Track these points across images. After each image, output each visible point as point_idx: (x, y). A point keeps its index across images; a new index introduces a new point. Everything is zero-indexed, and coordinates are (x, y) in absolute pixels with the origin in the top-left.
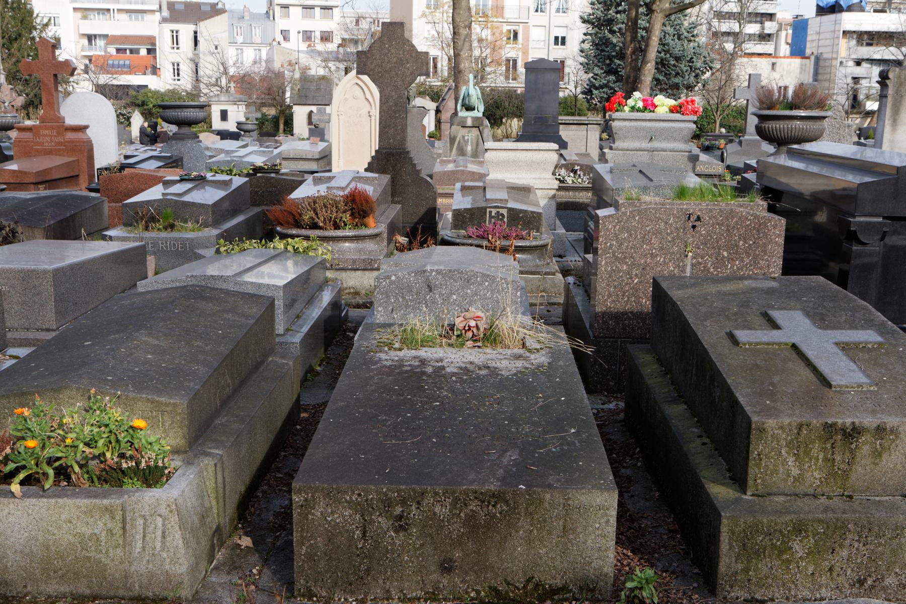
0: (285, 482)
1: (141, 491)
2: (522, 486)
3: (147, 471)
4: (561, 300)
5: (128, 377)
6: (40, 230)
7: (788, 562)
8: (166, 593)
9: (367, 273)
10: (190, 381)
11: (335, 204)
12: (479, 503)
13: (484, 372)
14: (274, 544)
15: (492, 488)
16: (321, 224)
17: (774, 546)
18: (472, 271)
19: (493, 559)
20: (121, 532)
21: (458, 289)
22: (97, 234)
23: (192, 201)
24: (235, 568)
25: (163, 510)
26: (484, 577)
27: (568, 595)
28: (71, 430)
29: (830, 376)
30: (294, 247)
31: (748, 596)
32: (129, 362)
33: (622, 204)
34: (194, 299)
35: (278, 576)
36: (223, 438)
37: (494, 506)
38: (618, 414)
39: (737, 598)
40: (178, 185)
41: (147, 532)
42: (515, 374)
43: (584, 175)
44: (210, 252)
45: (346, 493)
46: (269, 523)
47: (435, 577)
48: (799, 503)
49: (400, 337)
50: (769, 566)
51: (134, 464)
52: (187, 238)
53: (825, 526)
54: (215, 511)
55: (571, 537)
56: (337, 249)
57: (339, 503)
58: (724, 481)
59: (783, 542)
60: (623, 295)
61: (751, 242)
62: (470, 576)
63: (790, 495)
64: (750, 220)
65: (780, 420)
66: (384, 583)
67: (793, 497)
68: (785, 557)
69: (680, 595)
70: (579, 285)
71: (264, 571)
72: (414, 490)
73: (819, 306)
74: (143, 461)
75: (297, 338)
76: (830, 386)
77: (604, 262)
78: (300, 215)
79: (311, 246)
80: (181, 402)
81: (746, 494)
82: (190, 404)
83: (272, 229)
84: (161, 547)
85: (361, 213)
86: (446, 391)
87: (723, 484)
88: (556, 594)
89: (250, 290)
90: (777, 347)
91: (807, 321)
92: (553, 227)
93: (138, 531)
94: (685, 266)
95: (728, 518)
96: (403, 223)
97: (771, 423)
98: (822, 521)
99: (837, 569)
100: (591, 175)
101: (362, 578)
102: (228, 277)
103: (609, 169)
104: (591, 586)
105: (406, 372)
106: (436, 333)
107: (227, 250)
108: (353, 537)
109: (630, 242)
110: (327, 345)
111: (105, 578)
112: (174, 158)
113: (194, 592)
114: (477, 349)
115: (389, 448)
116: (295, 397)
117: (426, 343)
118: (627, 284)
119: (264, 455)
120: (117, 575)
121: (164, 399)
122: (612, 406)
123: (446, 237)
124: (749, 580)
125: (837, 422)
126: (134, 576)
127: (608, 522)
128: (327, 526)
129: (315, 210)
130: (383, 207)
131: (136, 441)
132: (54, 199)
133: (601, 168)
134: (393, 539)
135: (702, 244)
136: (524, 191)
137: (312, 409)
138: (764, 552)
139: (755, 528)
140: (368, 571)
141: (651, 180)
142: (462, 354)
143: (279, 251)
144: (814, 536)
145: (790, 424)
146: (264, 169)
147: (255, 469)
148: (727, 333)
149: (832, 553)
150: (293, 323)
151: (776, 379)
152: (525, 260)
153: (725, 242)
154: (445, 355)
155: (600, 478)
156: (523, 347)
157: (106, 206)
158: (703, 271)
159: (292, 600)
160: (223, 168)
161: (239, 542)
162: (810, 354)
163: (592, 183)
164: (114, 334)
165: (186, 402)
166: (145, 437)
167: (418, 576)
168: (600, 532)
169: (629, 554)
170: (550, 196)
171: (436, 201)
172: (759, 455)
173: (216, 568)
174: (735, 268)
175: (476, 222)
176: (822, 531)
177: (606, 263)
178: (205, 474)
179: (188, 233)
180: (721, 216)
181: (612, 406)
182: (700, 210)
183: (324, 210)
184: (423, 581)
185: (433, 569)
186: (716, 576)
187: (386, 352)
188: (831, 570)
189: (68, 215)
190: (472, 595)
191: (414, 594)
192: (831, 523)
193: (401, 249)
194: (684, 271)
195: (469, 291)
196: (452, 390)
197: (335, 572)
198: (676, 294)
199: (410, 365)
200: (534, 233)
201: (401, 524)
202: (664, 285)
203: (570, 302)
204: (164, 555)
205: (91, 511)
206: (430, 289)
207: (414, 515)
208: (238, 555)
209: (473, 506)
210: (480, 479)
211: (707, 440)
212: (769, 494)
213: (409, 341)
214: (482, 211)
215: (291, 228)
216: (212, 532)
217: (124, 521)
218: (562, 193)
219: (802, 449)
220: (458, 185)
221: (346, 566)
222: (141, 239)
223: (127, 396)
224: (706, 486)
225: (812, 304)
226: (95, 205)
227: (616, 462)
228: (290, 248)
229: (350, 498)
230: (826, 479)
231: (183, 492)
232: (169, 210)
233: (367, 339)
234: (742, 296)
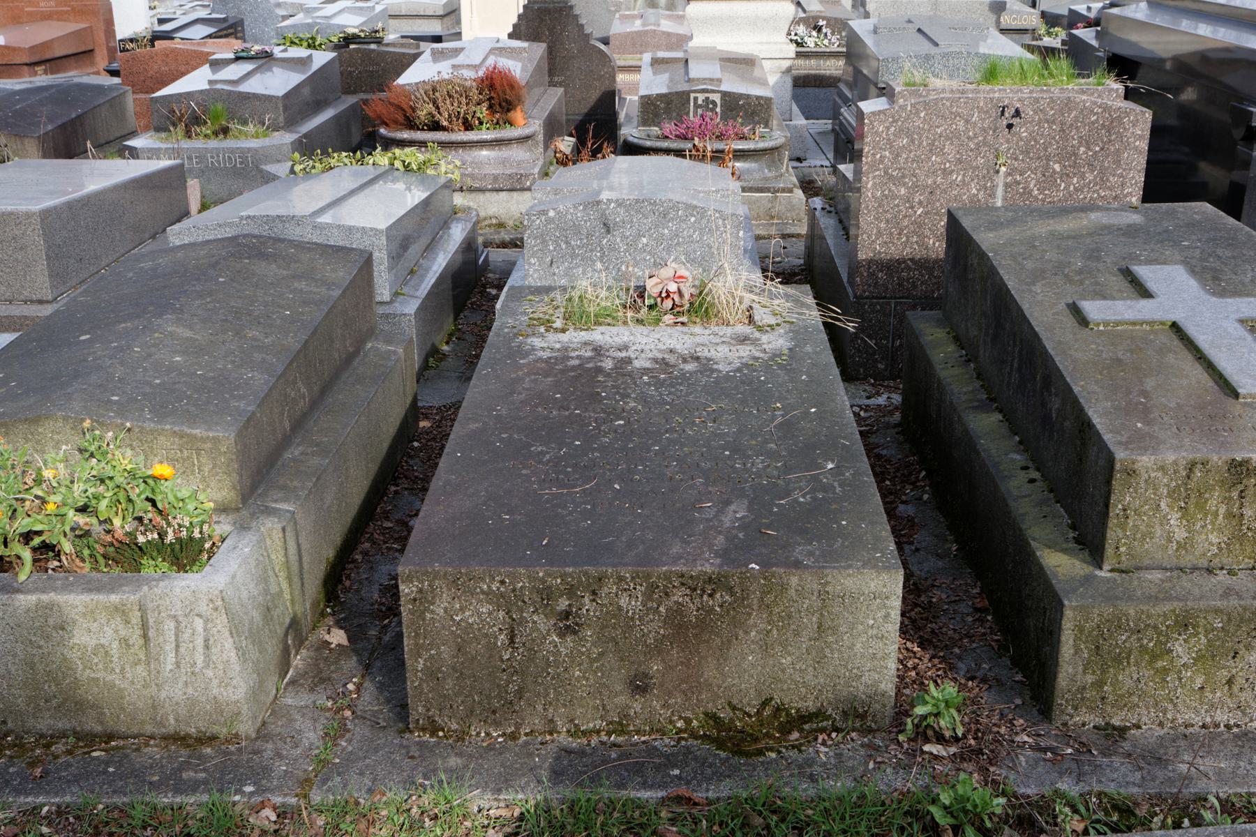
0: (396, 536)
1: (169, 577)
2: (753, 565)
3: (178, 547)
4: (803, 229)
5: (144, 395)
6: (32, 140)
7: (1165, 671)
8: (216, 729)
9: (515, 194)
10: (240, 398)
11: (465, 92)
12: (688, 592)
13: (690, 367)
14: (380, 639)
15: (708, 569)
16: (445, 123)
17: (1143, 649)
18: (670, 201)
19: (710, 672)
20: (141, 642)
21: (650, 228)
22: (116, 146)
23: (253, 91)
24: (322, 681)
25: (203, 607)
26: (697, 700)
27: (825, 723)
28: (52, 490)
29: (1236, 378)
30: (404, 162)
31: (1100, 721)
32: (145, 369)
33: (899, 93)
34: (249, 258)
35: (386, 694)
36: (295, 483)
37: (711, 595)
38: (891, 413)
39: (1084, 725)
40: (233, 67)
41: (181, 640)
42: (739, 370)
43: (833, 34)
44: (281, 169)
45: (482, 579)
46: (372, 605)
47: (621, 700)
48: (1185, 582)
49: (563, 310)
50: (1135, 678)
51: (156, 536)
52: (249, 149)
53: (1225, 618)
54: (288, 597)
55: (830, 639)
56: (470, 159)
57: (472, 594)
58: (1064, 546)
59: (1159, 642)
60: (900, 234)
61: (1097, 149)
62: (676, 698)
63: (1171, 570)
64: (1097, 113)
65: (1160, 457)
66: (544, 709)
67: (1175, 573)
68: (1160, 664)
69: (995, 719)
70: (830, 212)
71: (365, 685)
72: (586, 573)
73: (1210, 255)
74: (170, 531)
75: (410, 307)
76: (1236, 395)
77: (871, 183)
78: (414, 109)
79: (429, 161)
80: (225, 436)
81: (1101, 568)
82: (240, 435)
83: (374, 131)
84: (204, 661)
85: (504, 104)
86: (635, 399)
87: (1064, 551)
88: (806, 723)
89: (337, 240)
90: (1148, 328)
91: (1193, 282)
92: (787, 116)
93: (167, 639)
94: (994, 187)
95: (1074, 609)
96: (567, 115)
97: (1145, 461)
98: (1221, 611)
99: (1240, 681)
100: (844, 34)
101: (511, 703)
102: (302, 217)
103: (872, 28)
104: (861, 710)
105: (573, 368)
106: (617, 302)
107: (305, 169)
108: (495, 644)
109: (910, 152)
110: (458, 308)
111: (123, 709)
112: (231, 22)
113: (259, 724)
114: (679, 328)
115: (547, 501)
116: (409, 400)
117: (603, 318)
118: (905, 216)
119: (362, 496)
120: (140, 704)
121: (198, 431)
122: (881, 400)
123: (631, 139)
124: (1103, 698)
125: (1251, 458)
126: (167, 705)
127: (887, 616)
128: (454, 628)
129: (435, 102)
130: (537, 91)
131: (158, 498)
132: (53, 90)
133: (861, 26)
134: (556, 646)
135: (1022, 152)
136: (743, 63)
137: (437, 414)
138: (1128, 658)
139: (1117, 624)
140: (520, 693)
141: (936, 45)
142: (657, 336)
143: (381, 170)
144: (1207, 632)
145: (1175, 463)
146: (359, 37)
147: (350, 520)
148: (1068, 305)
149: (1234, 657)
150: (405, 283)
151: (1150, 384)
152: (748, 171)
153: (1057, 149)
154: (632, 338)
155: (876, 550)
156: (750, 322)
157: (130, 99)
158: (1022, 195)
159: (407, 735)
160: (301, 35)
161: (327, 637)
162: (1203, 340)
163: (848, 46)
164: (125, 321)
165: (233, 435)
166: (172, 490)
167: (595, 699)
168: (875, 632)
169: (916, 649)
170: (784, 69)
171: (614, 80)
172: (1125, 510)
173: (293, 682)
174: (1072, 188)
175: (674, 114)
176: (1220, 625)
177: (874, 184)
178: (269, 542)
179: (249, 140)
180: (1052, 109)
181: (881, 400)
182: (1019, 100)
183: (448, 102)
184: (604, 706)
185: (618, 688)
186: (1053, 693)
187: (542, 336)
188: (1230, 682)
189: (74, 116)
190: (679, 725)
191: (591, 725)
192: (1235, 614)
193: (563, 162)
194: (992, 195)
195: (666, 231)
196: (643, 399)
197: (470, 695)
198: (986, 239)
199: (578, 357)
200: (760, 129)
201: (568, 624)
202: (966, 223)
203: (817, 249)
204: (210, 673)
205: (92, 612)
206: (608, 228)
207: (587, 610)
208: (326, 659)
209: (678, 596)
210: (689, 554)
211: (1035, 475)
212: (1138, 568)
213: (577, 317)
214: (683, 97)
215: (401, 130)
216: (284, 629)
217: (144, 626)
218: (801, 62)
219: (1193, 500)
220: (647, 57)
221: (487, 685)
222: (176, 153)
223: (142, 428)
224: (1038, 554)
225: (1198, 251)
226: (114, 98)
227: (891, 493)
228: (398, 164)
229: (489, 587)
230: (1228, 545)
231: (234, 577)
232: (220, 106)
233: (514, 314)
234: (1088, 241)
